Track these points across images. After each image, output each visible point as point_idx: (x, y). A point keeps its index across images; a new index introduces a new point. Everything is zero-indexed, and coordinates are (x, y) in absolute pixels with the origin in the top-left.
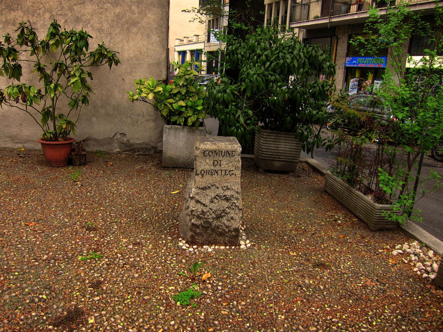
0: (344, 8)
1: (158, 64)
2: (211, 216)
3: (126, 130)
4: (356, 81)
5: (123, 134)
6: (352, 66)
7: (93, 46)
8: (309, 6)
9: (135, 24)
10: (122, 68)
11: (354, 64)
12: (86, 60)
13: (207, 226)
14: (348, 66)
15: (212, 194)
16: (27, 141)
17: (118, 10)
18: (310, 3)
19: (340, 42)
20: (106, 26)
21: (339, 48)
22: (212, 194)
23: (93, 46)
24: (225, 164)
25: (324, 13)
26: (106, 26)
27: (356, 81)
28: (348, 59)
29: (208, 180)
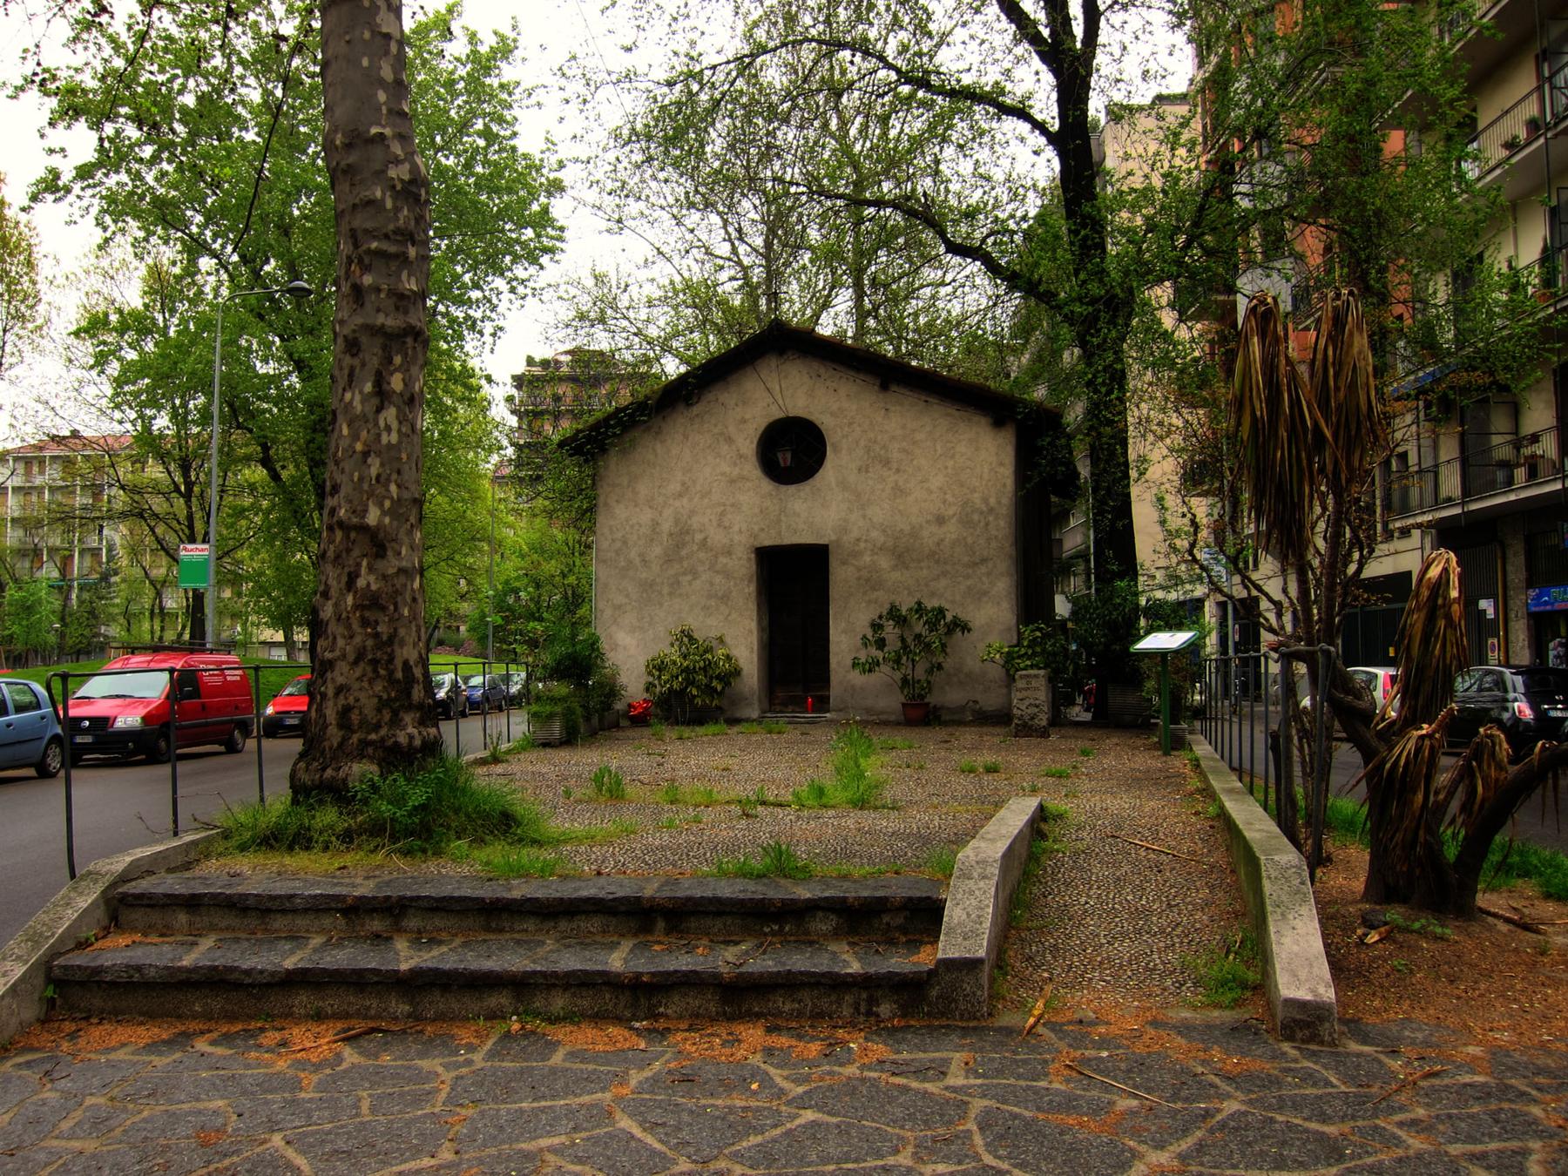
0: (1500, 475)
1: (1009, 629)
2: (1027, 718)
3: (978, 697)
4: (1560, 644)
5: (976, 702)
6: (1542, 608)
7: (949, 617)
8: (1436, 475)
9: (985, 593)
10: (973, 636)
11: (1546, 603)
12: (942, 630)
13: (1025, 725)
14: (1534, 609)
15: (1027, 702)
16: (882, 713)
17: (969, 583)
18: (1437, 466)
19: (1510, 554)
20: (958, 598)
21: (1509, 568)
22: (1027, 702)
23: (949, 617)
24: (1034, 683)
25: (1468, 492)
26: (958, 598)
27: (1560, 644)
28: (1532, 593)
29: (1024, 694)
